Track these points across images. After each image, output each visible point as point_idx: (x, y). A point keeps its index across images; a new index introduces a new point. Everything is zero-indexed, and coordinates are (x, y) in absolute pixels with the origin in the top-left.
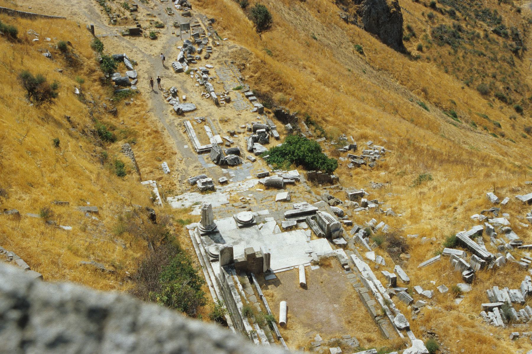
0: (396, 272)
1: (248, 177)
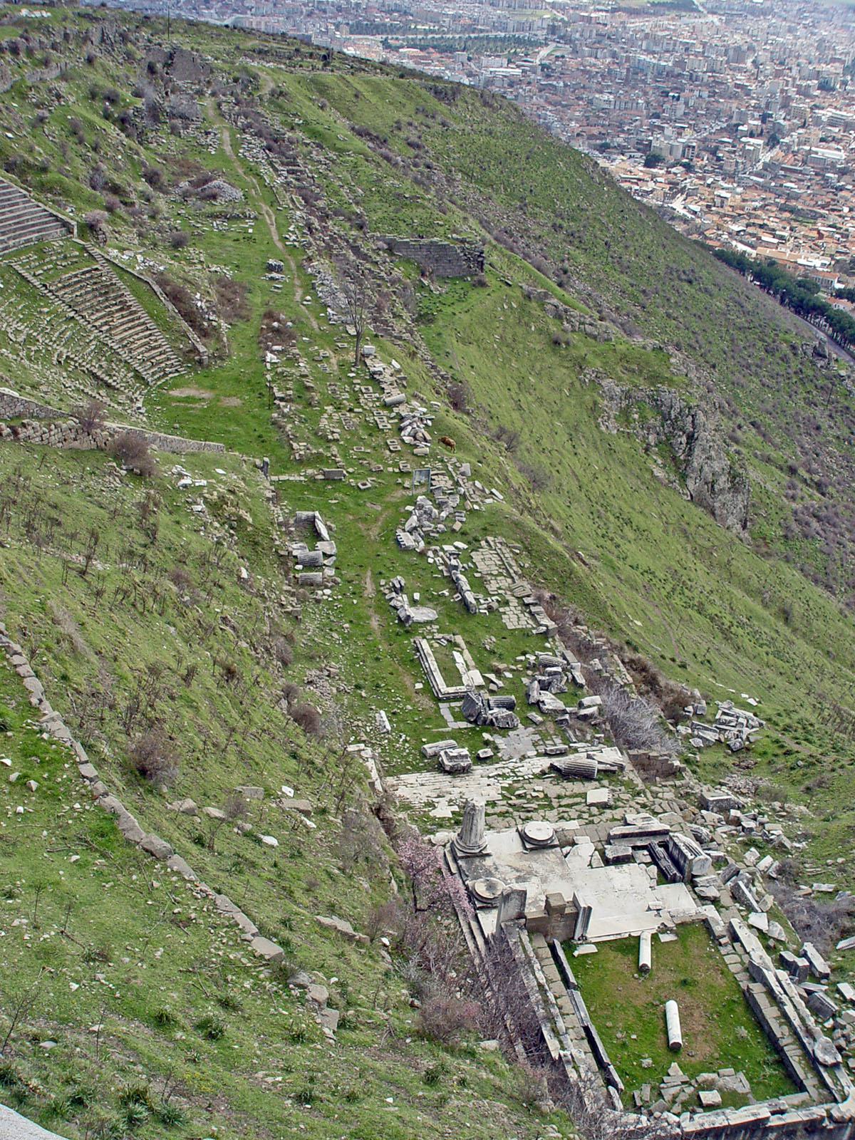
0: (805, 955)
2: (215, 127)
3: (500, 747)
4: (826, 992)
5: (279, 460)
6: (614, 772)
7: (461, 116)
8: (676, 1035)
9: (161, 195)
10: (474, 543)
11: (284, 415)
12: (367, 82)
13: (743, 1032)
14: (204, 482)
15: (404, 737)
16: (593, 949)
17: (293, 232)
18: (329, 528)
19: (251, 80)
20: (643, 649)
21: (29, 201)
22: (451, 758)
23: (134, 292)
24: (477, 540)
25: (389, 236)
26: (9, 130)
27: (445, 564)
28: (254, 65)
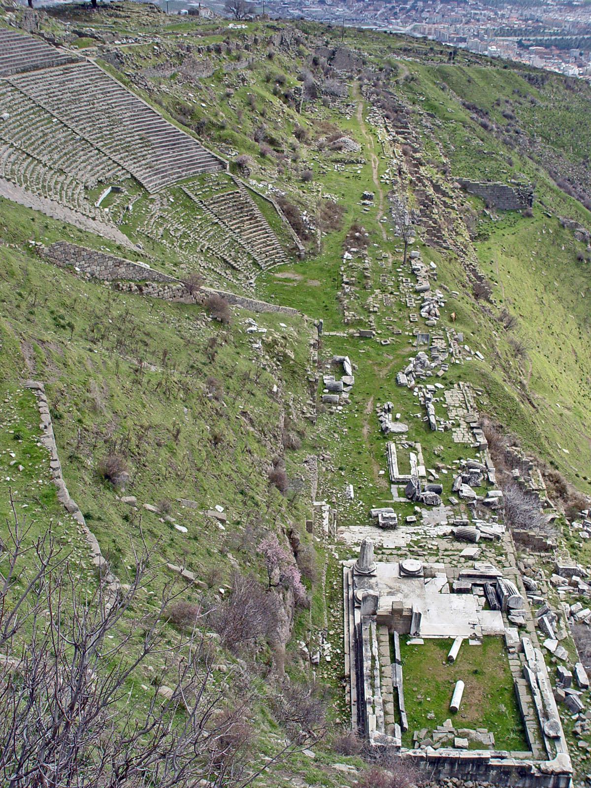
2: (355, 101)
3: (423, 516)
4: (580, 696)
5: (334, 322)
6: (491, 540)
7: (547, 98)
8: (456, 702)
9: (305, 146)
10: (449, 385)
11: (345, 294)
12: (479, 72)
13: (503, 708)
14: (265, 330)
15: (361, 502)
16: (421, 642)
17: (388, 174)
18: (353, 368)
19: (393, 70)
20: (563, 468)
21: (200, 147)
22: (384, 518)
23: (261, 208)
24: (452, 383)
25: (465, 179)
26: (204, 101)
27: (424, 397)
28: (397, 59)
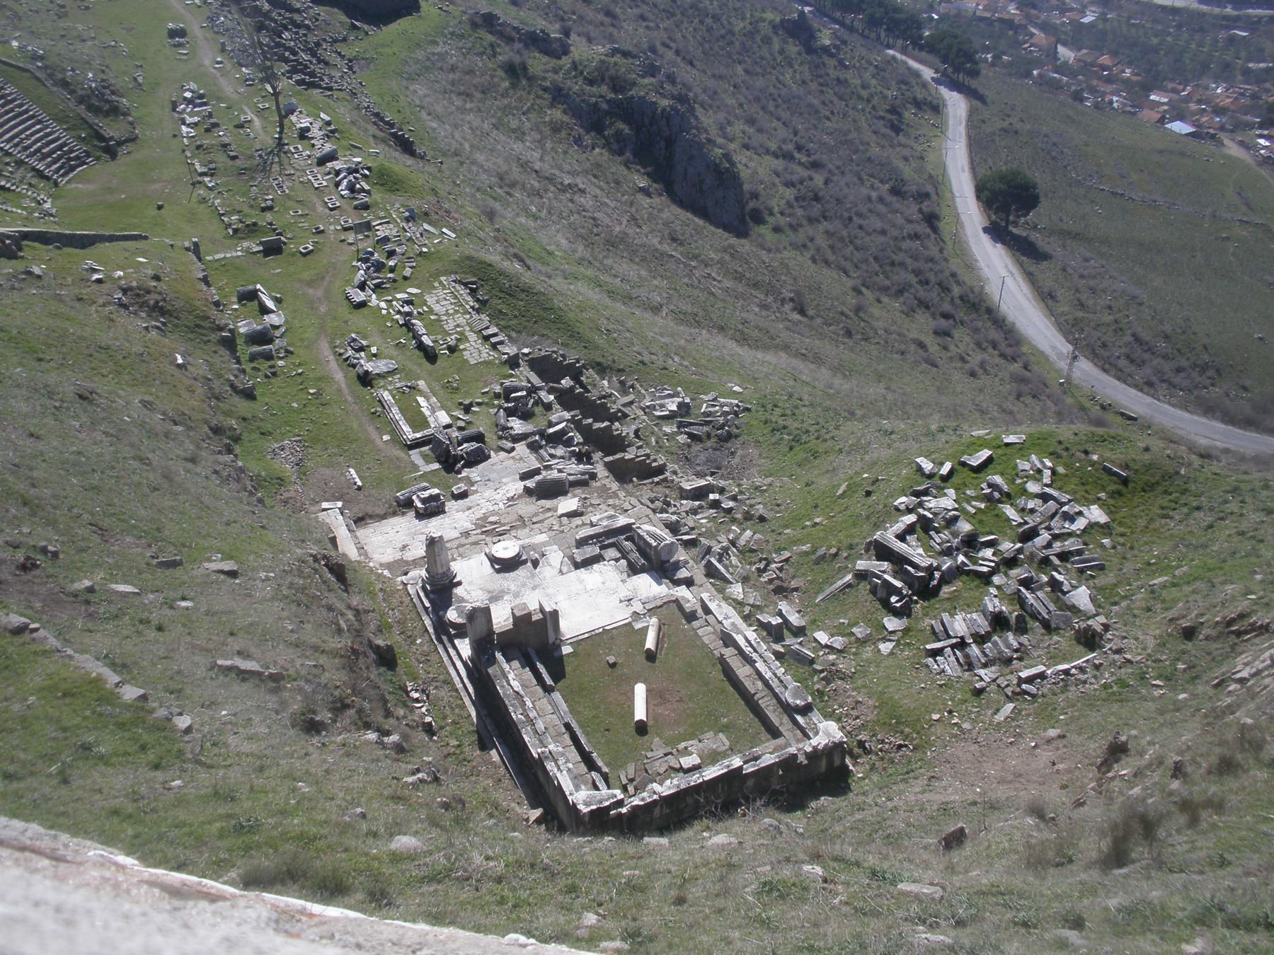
0: (780, 614)
1: (504, 480)
8: (640, 713)
